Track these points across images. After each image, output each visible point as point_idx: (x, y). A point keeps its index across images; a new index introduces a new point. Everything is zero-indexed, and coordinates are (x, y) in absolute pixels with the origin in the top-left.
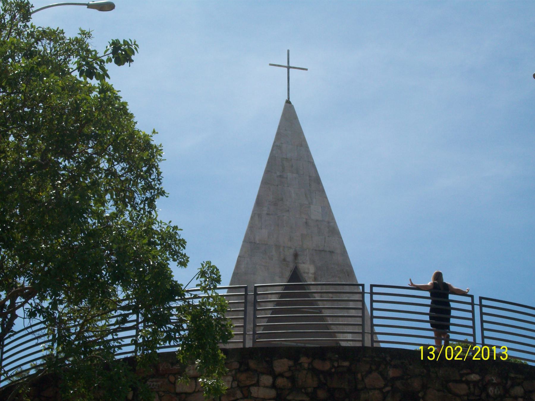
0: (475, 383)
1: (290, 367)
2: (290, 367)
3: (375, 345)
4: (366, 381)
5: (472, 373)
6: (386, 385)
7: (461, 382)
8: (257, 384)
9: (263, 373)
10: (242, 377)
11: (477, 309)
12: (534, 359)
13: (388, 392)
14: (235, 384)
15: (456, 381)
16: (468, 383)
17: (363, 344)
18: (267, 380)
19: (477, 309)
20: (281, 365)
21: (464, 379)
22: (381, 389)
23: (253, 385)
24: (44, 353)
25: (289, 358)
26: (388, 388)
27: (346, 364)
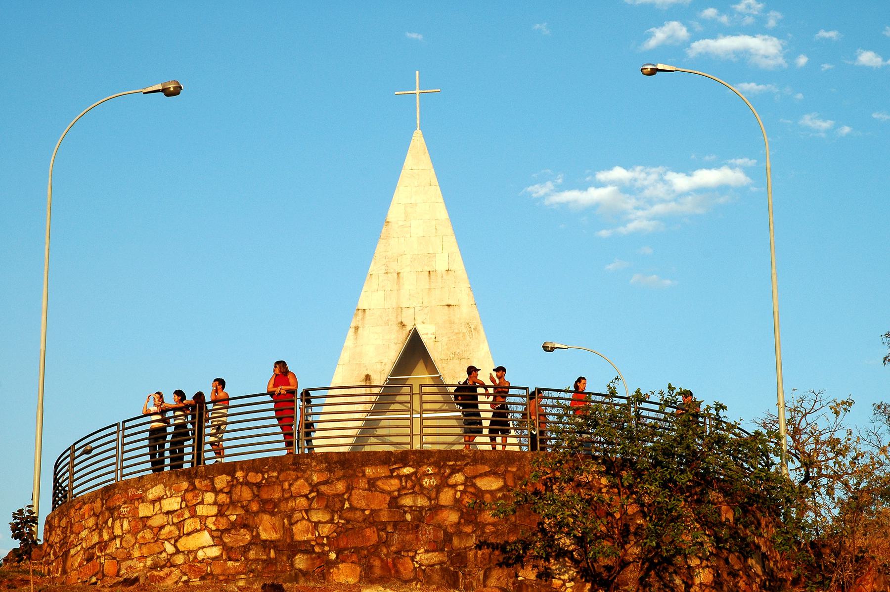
0: (407, 477)
1: (228, 482)
2: (228, 482)
4: (292, 489)
5: (405, 466)
7: (391, 477)
8: (202, 503)
9: (207, 491)
10: (189, 496)
13: (314, 498)
14: (183, 505)
15: (386, 477)
16: (399, 477)
18: (209, 497)
19: (416, 430)
20: (462, 521)
21: (395, 474)
22: (306, 496)
23: (198, 504)
25: (228, 474)
26: (314, 494)
27: (275, 474)
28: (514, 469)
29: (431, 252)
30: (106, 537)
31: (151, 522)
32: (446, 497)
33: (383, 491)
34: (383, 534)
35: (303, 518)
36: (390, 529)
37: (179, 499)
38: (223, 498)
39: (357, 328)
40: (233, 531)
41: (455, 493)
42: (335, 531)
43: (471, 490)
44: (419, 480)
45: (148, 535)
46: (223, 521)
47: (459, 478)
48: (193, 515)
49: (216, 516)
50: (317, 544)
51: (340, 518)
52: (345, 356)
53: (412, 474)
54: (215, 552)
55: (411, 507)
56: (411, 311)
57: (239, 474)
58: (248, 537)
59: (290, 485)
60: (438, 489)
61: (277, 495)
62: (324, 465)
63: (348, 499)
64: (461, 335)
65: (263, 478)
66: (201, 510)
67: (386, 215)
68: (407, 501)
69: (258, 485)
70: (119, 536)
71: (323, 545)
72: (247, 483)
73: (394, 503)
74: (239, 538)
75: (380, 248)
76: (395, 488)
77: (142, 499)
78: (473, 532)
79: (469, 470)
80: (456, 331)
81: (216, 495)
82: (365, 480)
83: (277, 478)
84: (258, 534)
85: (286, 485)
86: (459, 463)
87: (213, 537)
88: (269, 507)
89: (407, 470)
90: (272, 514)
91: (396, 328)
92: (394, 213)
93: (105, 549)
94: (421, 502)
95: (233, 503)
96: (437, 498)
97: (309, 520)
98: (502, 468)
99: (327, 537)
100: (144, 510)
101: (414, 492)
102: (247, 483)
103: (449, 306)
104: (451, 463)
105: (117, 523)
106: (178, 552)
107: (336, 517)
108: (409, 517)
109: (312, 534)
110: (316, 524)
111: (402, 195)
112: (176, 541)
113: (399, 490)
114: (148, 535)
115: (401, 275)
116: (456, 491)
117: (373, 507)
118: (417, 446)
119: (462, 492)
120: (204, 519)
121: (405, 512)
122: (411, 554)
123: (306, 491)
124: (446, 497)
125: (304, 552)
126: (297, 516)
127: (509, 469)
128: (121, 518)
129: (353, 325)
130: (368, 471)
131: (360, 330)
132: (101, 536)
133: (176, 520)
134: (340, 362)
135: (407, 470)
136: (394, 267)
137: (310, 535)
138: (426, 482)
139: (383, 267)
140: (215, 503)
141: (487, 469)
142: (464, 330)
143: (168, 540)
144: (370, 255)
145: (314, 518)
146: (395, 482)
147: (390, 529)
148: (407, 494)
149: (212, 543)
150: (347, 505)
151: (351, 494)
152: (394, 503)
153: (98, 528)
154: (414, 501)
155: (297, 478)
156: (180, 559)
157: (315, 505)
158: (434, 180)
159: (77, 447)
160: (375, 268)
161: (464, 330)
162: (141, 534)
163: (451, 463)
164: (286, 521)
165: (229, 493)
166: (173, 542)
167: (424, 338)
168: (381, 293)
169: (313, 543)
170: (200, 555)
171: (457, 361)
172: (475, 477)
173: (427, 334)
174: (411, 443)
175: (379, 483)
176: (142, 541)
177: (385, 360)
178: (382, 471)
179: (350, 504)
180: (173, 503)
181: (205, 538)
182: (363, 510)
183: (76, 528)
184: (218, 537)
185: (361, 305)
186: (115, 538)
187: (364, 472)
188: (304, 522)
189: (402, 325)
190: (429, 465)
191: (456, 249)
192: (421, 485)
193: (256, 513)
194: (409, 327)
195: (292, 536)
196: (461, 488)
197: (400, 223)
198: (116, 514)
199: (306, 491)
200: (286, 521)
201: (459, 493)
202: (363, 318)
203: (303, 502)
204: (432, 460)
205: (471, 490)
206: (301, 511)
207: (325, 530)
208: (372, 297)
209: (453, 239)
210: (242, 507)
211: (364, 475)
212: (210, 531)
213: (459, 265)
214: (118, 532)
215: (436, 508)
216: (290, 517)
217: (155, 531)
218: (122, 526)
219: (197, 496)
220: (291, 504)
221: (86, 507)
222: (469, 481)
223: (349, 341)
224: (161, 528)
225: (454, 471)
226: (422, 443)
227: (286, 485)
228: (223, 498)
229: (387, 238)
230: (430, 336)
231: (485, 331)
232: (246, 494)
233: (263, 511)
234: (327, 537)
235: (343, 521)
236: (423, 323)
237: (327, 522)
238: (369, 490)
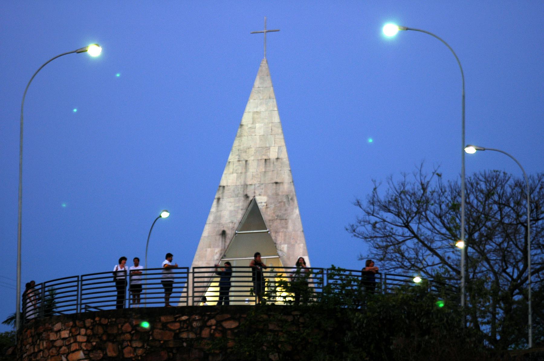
0: (184, 321)
1: (92, 323)
2: (92, 323)
3: (195, 304)
5: (183, 316)
6: (132, 330)
7: (175, 321)
8: (79, 334)
9: (81, 328)
10: (73, 330)
11: (190, 294)
12: (520, 167)
13: (134, 333)
14: (71, 335)
15: (172, 322)
16: (180, 322)
17: (187, 304)
18: (83, 331)
19: (190, 294)
21: (177, 320)
22: (130, 333)
24: (402, 283)
25: (92, 319)
26: (133, 332)
27: (114, 320)
28: (245, 316)
29: (268, 146)
30: (36, 350)
32: (206, 333)
33: (170, 330)
34: (171, 354)
36: (174, 351)
37: (68, 332)
38: (89, 332)
39: (219, 199)
40: (94, 351)
41: (210, 331)
42: (145, 353)
43: (220, 328)
44: (190, 324)
45: (54, 351)
46: (90, 345)
47: (213, 322)
49: (86, 342)
51: (148, 345)
52: (211, 218)
53: (187, 320)
55: (186, 339)
56: (253, 187)
57: (97, 319)
58: (101, 355)
59: (122, 326)
60: (201, 328)
61: (115, 331)
62: (139, 315)
64: (282, 204)
66: (80, 339)
67: (241, 120)
68: (184, 335)
72: (100, 324)
73: (177, 336)
74: (97, 355)
75: (236, 143)
77: (51, 330)
78: (220, 353)
79: (218, 317)
80: (280, 200)
81: (86, 330)
82: (161, 324)
83: (115, 321)
84: (106, 354)
85: (120, 326)
86: (213, 313)
88: (112, 338)
89: (184, 318)
90: (113, 342)
91: (243, 199)
92: (246, 119)
94: (192, 336)
95: (94, 335)
96: (200, 333)
97: (131, 346)
98: (238, 315)
99: (141, 356)
100: (53, 337)
101: (187, 330)
102: (100, 324)
103: (276, 183)
104: (208, 313)
107: (145, 345)
108: (185, 344)
109: (134, 354)
110: (135, 349)
111: (252, 106)
112: (67, 355)
113: (179, 329)
115: (248, 162)
116: (211, 329)
117: (165, 339)
118: (190, 303)
119: (215, 330)
120: (80, 343)
121: (183, 342)
123: (129, 329)
124: (206, 333)
126: (125, 344)
127: (242, 316)
128: (42, 340)
129: (216, 197)
130: (163, 319)
131: (221, 200)
132: (34, 349)
133: (67, 343)
134: (208, 222)
135: (184, 318)
136: (244, 156)
138: (195, 324)
139: (237, 157)
140: (86, 335)
141: (229, 316)
142: (285, 200)
144: (228, 149)
145: (134, 345)
146: (177, 325)
147: (174, 351)
148: (184, 331)
149: (84, 357)
150: (151, 338)
151: (153, 332)
152: (177, 336)
153: (33, 344)
154: (188, 335)
155: (125, 323)
157: (134, 338)
158: (273, 95)
159: (47, 284)
160: (232, 157)
161: (285, 200)
162: (51, 350)
163: (208, 313)
164: (120, 346)
165: (92, 329)
166: (65, 356)
167: (260, 205)
168: (235, 175)
171: (279, 221)
172: (222, 321)
173: (262, 203)
174: (187, 302)
175: (169, 325)
176: (52, 354)
177: (235, 221)
178: (170, 318)
179: (153, 337)
180: (65, 334)
182: (160, 341)
185: (223, 183)
187: (160, 319)
188: (129, 348)
189: (247, 197)
190: (196, 315)
191: (283, 143)
192: (192, 326)
193: (105, 342)
194: (251, 198)
195: (123, 354)
196: (214, 327)
197: (250, 126)
198: (41, 337)
199: (129, 329)
200: (120, 346)
201: (212, 331)
202: (223, 192)
203: (128, 336)
205: (220, 328)
206: (127, 341)
207: (140, 352)
208: (229, 178)
209: (282, 136)
210: (99, 338)
211: (160, 321)
212: (84, 351)
213: (284, 156)
214: (41, 348)
215: (200, 339)
216: (122, 344)
217: (58, 349)
218: (43, 345)
219: (76, 330)
220: (123, 337)
222: (219, 323)
223: (213, 209)
225: (211, 317)
226: (194, 302)
227: (120, 326)
229: (241, 136)
230: (263, 204)
231: (298, 200)
232: (100, 331)
233: (108, 340)
235: (148, 347)
236: (260, 195)
237: (141, 348)
238: (162, 329)
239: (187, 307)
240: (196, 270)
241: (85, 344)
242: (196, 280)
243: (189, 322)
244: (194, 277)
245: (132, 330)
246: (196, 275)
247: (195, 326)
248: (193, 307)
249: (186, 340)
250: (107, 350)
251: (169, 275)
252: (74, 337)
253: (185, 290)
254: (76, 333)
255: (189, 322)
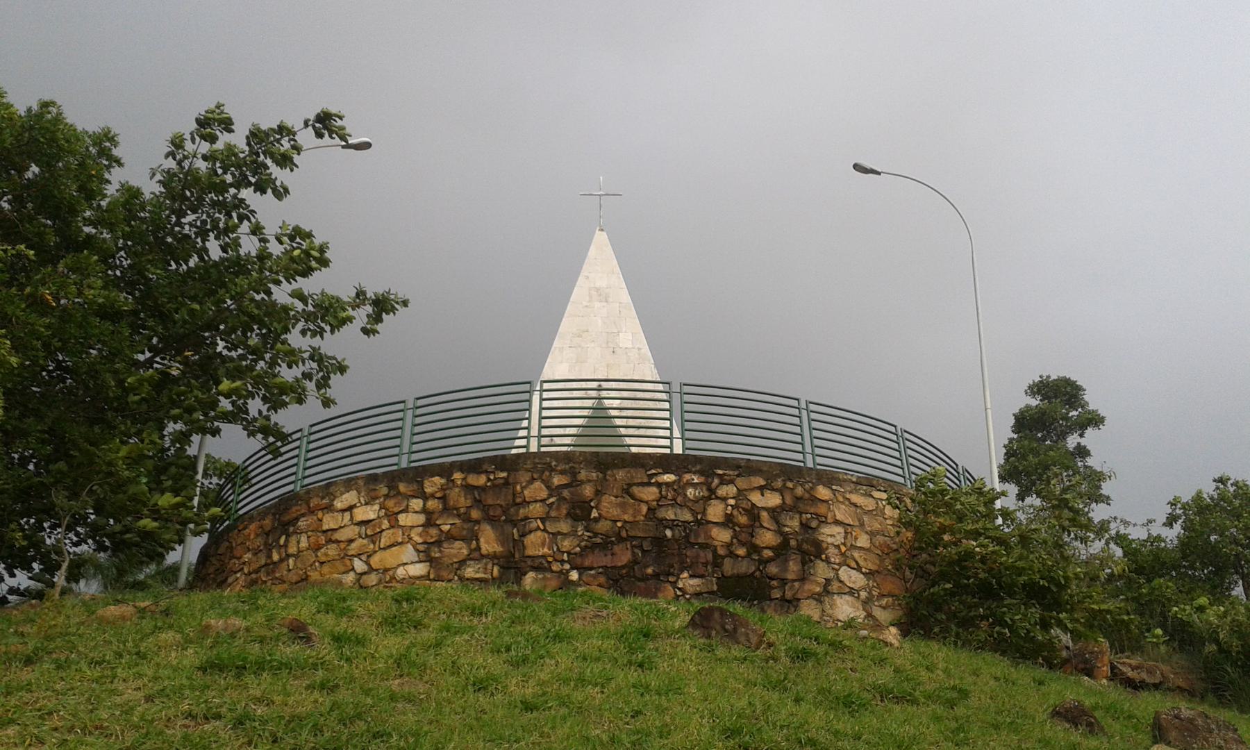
0: (667, 484)
6: (550, 496)
7: (649, 484)
8: (406, 511)
10: (390, 503)
11: (534, 432)
15: (642, 484)
16: (659, 485)
23: (401, 512)
25: (441, 476)
26: (552, 500)
31: (337, 536)
32: (715, 512)
35: (538, 528)
48: (394, 525)
49: (422, 526)
50: (556, 560)
51: (587, 529)
54: (418, 569)
63: (596, 507)
65: (489, 480)
68: (670, 514)
69: (483, 489)
70: (293, 555)
71: (562, 562)
76: (653, 497)
77: (329, 508)
79: (742, 483)
84: (478, 548)
87: (418, 551)
93: (274, 572)
95: (447, 509)
97: (545, 530)
100: (329, 522)
105: (293, 540)
106: (371, 570)
112: (369, 556)
114: (332, 551)
122: (671, 579)
125: (537, 569)
132: (269, 556)
135: (669, 478)
137: (546, 550)
138: (690, 492)
143: (358, 556)
156: (372, 579)
163: (720, 472)
166: (364, 558)
169: (550, 559)
170: (401, 572)
174: (671, 447)
180: (369, 513)
181: (408, 553)
183: (237, 553)
184: (426, 555)
186: (288, 556)
188: (539, 533)
190: (694, 473)
193: (477, 522)
196: (732, 502)
204: (698, 467)
218: (298, 542)
221: (252, 527)
222: (741, 494)
224: (351, 541)
225: (723, 482)
226: (540, 446)
228: (432, 504)
234: (569, 553)
239: (528, 455)
240: (546, 386)
241: (421, 529)
242: (545, 404)
243: (678, 487)
244: (542, 400)
245: (550, 496)
246: (545, 395)
247: (691, 497)
248: (539, 454)
249: (673, 525)
250: (482, 540)
251: (280, 459)
252: (392, 517)
253: (525, 424)
254: (396, 510)
255: (678, 487)
